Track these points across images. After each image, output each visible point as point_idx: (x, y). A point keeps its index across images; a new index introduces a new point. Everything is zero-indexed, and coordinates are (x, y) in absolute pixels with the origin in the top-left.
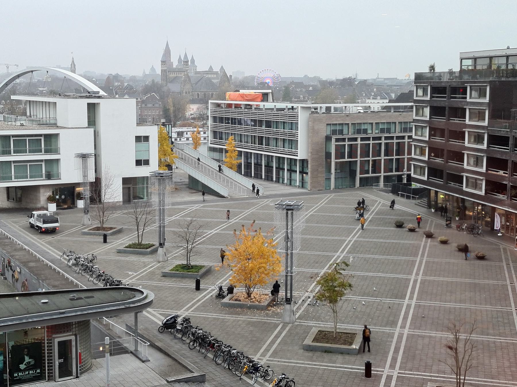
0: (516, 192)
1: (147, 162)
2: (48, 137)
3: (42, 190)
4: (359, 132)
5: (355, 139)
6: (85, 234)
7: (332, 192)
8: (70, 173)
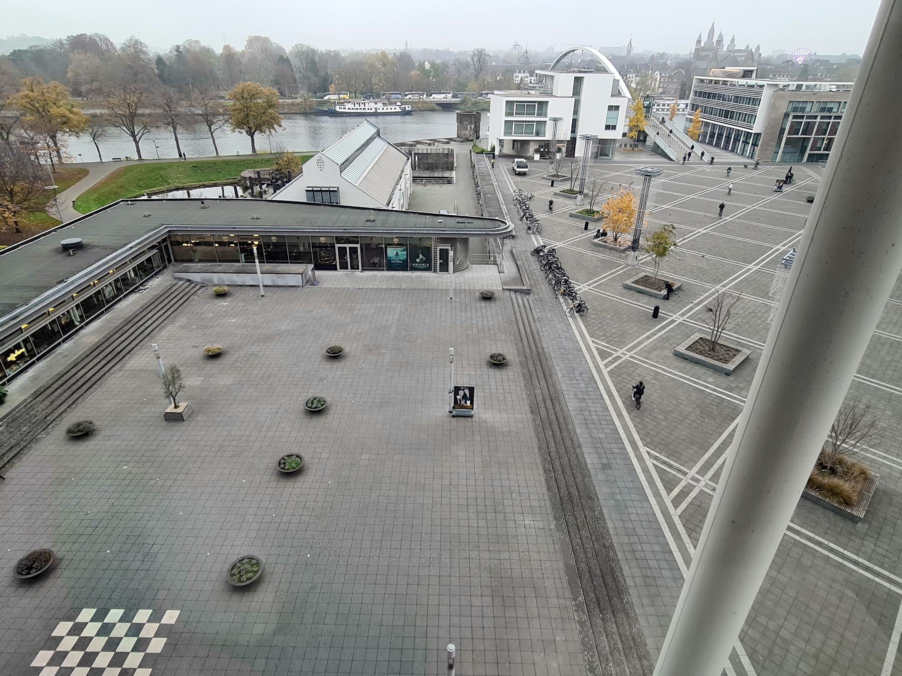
1: (614, 127)
2: (541, 104)
3: (531, 144)
4: (822, 110)
5: (816, 117)
6: (543, 178)
7: (777, 164)
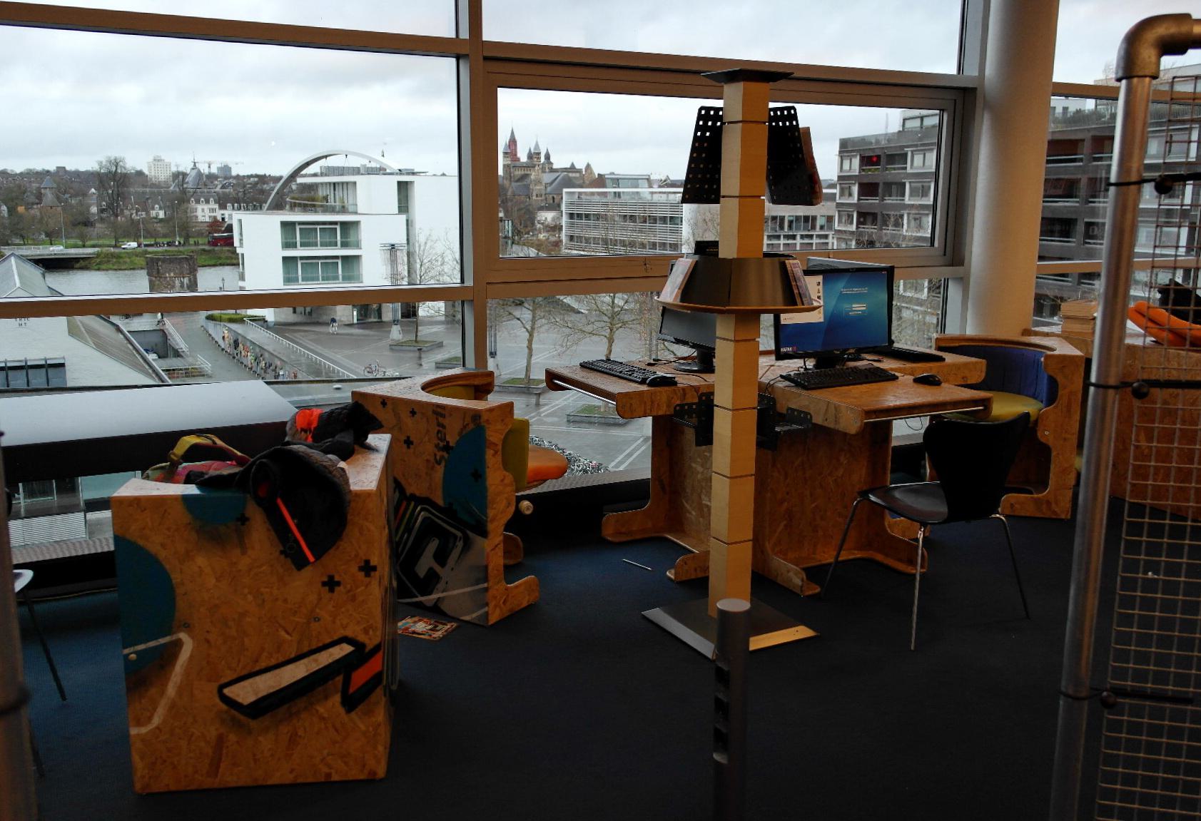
0: (1200, 344)
8: (374, 274)
